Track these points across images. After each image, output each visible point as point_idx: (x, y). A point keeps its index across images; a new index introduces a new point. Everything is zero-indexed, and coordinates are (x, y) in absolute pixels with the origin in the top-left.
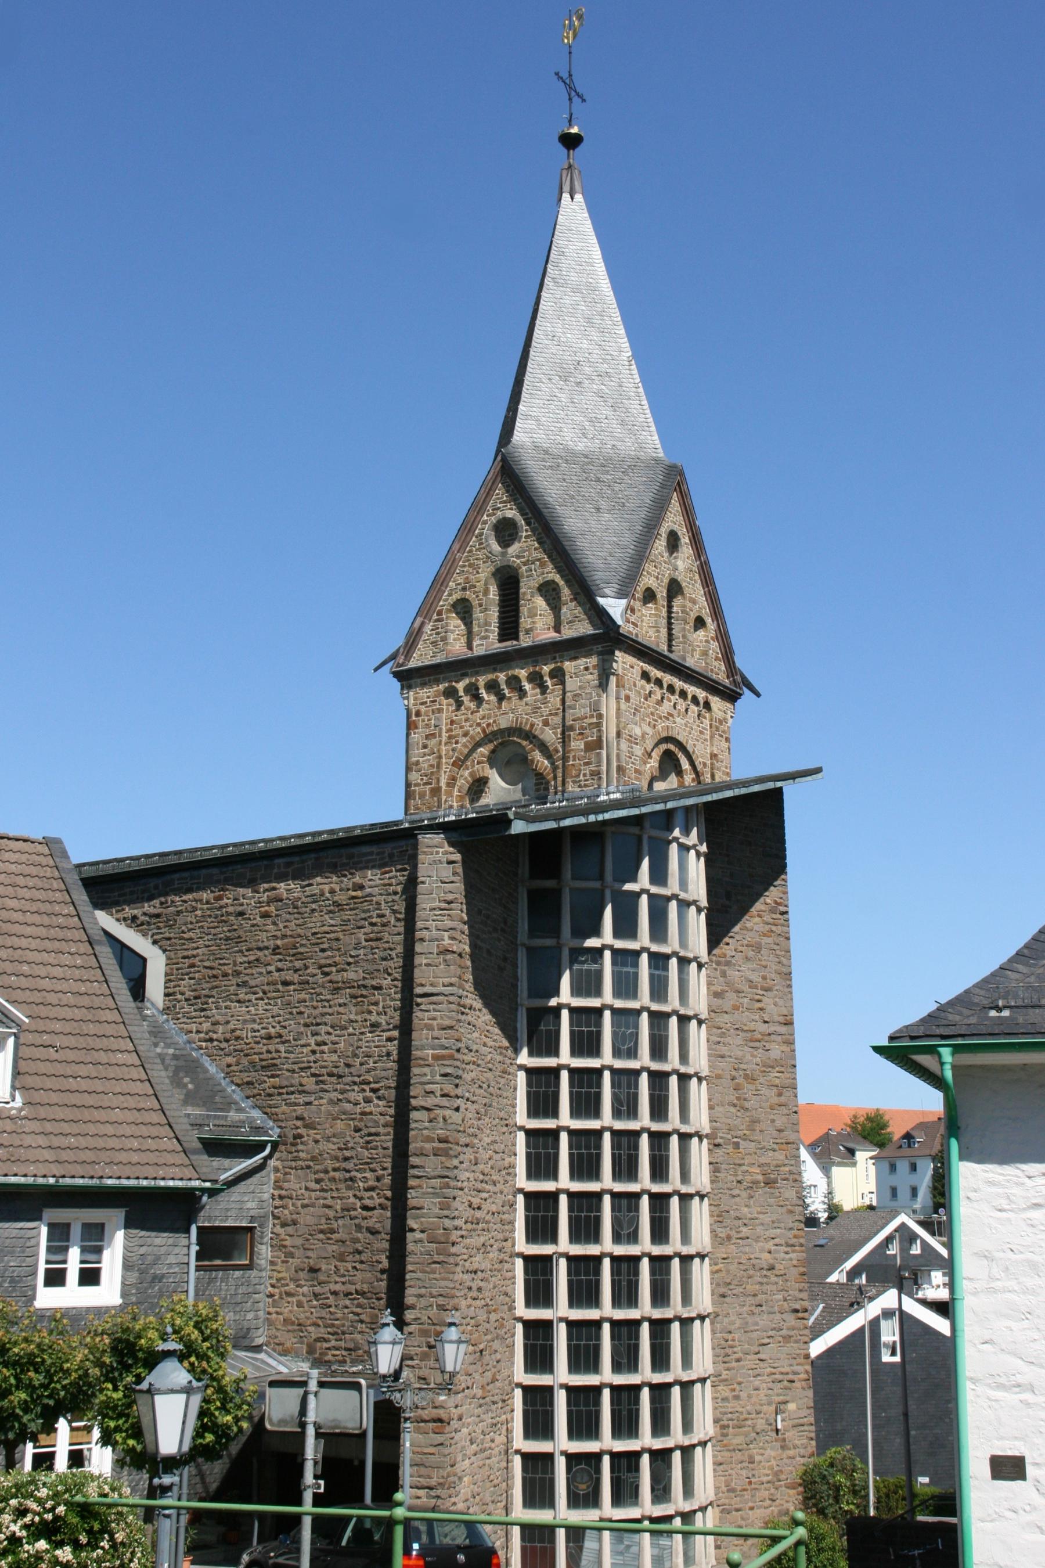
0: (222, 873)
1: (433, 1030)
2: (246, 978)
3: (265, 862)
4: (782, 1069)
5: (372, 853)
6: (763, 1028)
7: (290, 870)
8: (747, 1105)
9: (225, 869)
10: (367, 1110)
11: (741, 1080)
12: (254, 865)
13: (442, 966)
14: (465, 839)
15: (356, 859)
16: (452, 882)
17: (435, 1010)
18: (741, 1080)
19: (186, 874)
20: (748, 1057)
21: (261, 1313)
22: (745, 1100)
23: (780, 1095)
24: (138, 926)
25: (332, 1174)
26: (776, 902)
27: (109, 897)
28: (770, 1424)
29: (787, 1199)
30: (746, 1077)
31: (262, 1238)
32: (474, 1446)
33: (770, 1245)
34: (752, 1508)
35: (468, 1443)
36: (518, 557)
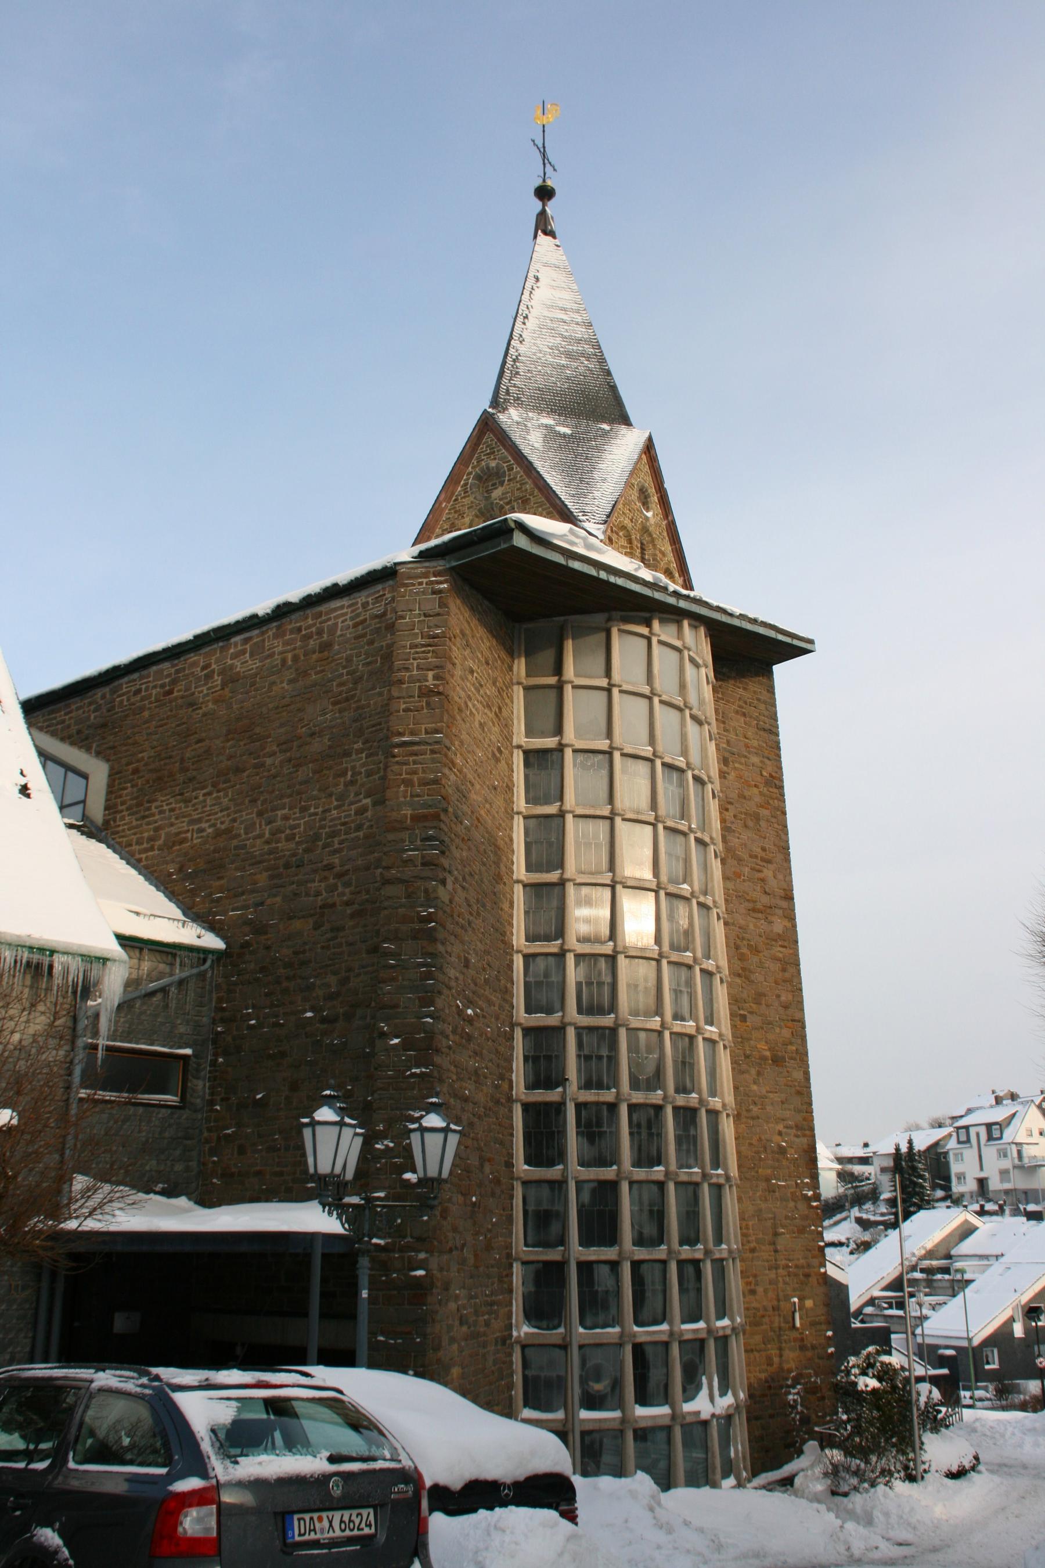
0: (173, 666)
1: (413, 786)
2: (194, 773)
3: (221, 644)
4: (786, 944)
5: (342, 607)
6: (765, 900)
7: (248, 646)
8: (753, 977)
9: (176, 662)
10: (330, 901)
11: (745, 950)
12: (208, 649)
13: (425, 711)
14: (454, 564)
15: (324, 618)
16: (438, 614)
17: (415, 763)
18: (745, 950)
19: (136, 676)
20: (751, 926)
21: (194, 1164)
22: (750, 972)
23: (784, 970)
24: (82, 741)
25: (285, 984)
26: (771, 776)
27: (55, 718)
28: (787, 1322)
29: (796, 1080)
30: (749, 946)
31: (198, 1070)
32: (465, 1328)
33: (780, 1127)
34: (772, 1416)
35: (457, 1323)
36: (501, 500)
